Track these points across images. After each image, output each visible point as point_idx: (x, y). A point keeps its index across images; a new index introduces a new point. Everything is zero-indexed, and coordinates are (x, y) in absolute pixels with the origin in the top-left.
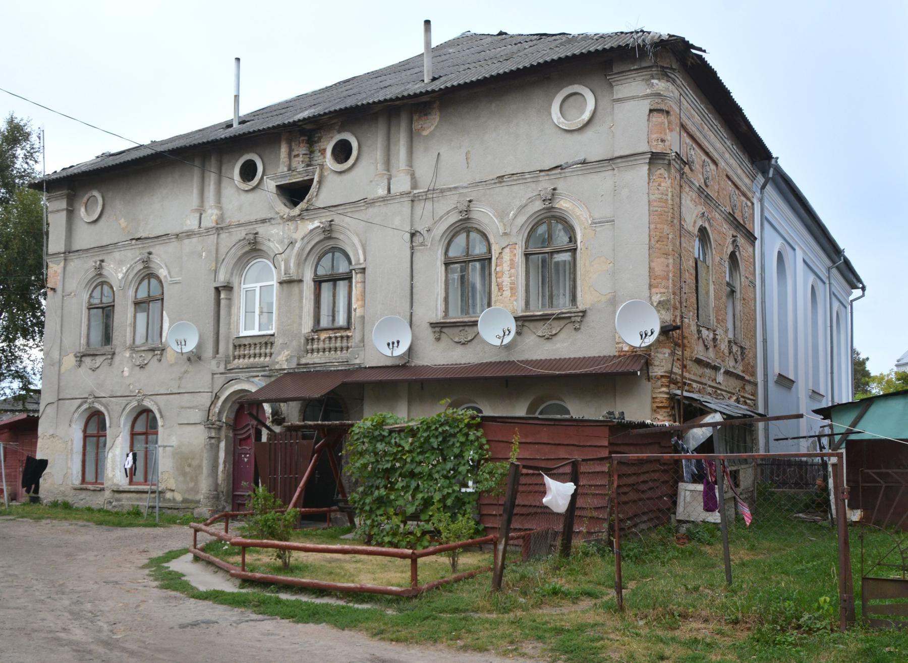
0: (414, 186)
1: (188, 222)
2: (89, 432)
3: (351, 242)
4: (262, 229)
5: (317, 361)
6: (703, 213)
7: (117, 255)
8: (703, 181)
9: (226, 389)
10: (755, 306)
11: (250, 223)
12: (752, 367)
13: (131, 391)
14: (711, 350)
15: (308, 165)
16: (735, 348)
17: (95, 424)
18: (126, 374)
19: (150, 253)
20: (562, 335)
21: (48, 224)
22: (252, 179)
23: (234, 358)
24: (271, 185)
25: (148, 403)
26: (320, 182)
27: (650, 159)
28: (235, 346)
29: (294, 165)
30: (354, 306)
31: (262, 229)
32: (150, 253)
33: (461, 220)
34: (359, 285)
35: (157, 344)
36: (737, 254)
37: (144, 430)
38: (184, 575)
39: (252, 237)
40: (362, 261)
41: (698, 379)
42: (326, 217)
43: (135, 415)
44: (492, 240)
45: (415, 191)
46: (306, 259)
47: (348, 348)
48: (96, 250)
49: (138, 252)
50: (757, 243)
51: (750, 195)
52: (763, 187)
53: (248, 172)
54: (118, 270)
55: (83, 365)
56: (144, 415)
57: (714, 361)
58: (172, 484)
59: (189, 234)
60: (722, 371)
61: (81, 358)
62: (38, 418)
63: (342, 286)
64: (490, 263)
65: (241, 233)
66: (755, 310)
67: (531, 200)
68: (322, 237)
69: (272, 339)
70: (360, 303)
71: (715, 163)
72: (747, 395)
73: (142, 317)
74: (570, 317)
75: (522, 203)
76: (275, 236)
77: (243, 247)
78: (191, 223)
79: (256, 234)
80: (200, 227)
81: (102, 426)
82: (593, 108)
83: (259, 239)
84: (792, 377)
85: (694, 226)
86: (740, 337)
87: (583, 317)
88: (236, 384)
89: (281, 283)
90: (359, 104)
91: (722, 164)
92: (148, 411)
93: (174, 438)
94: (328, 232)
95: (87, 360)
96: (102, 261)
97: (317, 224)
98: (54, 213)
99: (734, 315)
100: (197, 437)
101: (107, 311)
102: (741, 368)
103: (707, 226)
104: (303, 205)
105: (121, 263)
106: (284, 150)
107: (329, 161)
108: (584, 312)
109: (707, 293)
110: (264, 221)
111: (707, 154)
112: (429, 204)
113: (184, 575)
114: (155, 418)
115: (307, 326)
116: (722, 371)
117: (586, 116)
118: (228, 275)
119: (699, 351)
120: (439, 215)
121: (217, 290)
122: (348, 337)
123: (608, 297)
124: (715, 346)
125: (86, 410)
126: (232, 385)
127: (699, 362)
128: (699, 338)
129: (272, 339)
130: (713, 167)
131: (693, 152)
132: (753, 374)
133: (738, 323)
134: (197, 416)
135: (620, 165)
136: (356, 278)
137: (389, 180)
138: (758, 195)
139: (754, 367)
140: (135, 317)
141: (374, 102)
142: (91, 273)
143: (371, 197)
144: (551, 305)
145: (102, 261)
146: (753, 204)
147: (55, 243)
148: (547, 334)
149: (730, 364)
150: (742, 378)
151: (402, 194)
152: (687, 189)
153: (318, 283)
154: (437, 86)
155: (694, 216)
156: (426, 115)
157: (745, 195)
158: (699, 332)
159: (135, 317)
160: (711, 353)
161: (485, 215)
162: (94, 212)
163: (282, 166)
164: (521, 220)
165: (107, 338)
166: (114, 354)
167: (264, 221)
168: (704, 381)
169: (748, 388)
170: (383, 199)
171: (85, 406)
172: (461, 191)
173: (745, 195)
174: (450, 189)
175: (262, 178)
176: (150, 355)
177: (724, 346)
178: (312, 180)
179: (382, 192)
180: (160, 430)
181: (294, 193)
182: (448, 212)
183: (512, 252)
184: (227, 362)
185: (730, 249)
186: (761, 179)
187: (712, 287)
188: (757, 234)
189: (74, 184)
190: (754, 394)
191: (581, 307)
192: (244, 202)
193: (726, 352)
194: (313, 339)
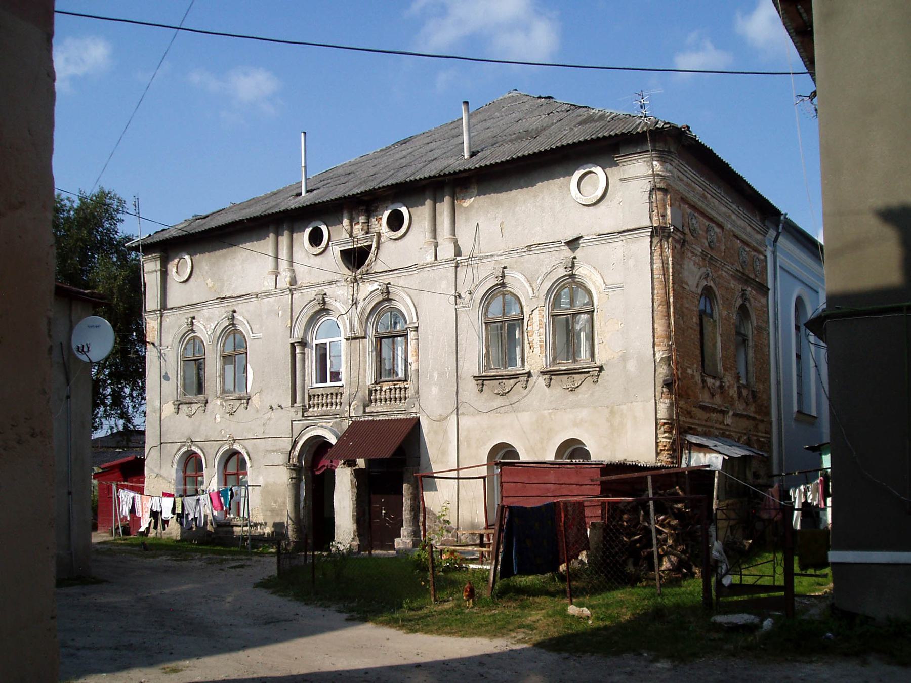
0: (458, 253)
1: (266, 283)
2: (188, 473)
3: (403, 303)
4: (328, 290)
5: (380, 409)
6: (708, 274)
7: (206, 312)
8: (707, 244)
9: (304, 434)
10: (769, 351)
11: (319, 285)
12: (766, 407)
13: (223, 436)
14: (717, 396)
15: (367, 233)
16: (745, 392)
17: (191, 464)
18: (218, 420)
19: (234, 311)
20: (583, 387)
21: (145, 284)
22: (320, 245)
23: (310, 407)
24: (336, 250)
25: (237, 447)
26: (378, 248)
27: (652, 232)
28: (310, 396)
29: (355, 232)
30: (410, 361)
31: (328, 290)
32: (234, 311)
33: (497, 285)
34: (414, 342)
35: (243, 394)
36: (748, 305)
37: (235, 471)
38: (347, 620)
39: (321, 297)
40: (415, 320)
41: (704, 423)
42: (385, 279)
43: (227, 457)
44: (524, 304)
45: (458, 258)
46: (368, 318)
47: (406, 398)
48: (187, 307)
49: (223, 310)
50: (771, 293)
51: (762, 249)
52: (776, 240)
53: (316, 238)
54: (207, 327)
55: (180, 411)
56: (235, 458)
57: (719, 406)
58: (260, 519)
59: (267, 294)
60: (731, 413)
61: (178, 406)
62: (144, 460)
63: (470, 268)
64: (523, 323)
65: (312, 293)
66: (769, 355)
67: (555, 268)
68: (381, 298)
69: (341, 390)
70: (414, 358)
71: (720, 226)
72: (760, 434)
73: (229, 369)
74: (588, 372)
75: (552, 264)
76: (339, 296)
77: (314, 306)
78: (269, 284)
79: (325, 294)
80: (436, 258)
81: (199, 467)
82: (605, 185)
83: (327, 300)
84: (814, 414)
85: (697, 287)
86: (752, 381)
87: (529, 377)
88: (312, 430)
89: (347, 339)
90: (408, 180)
91: (728, 226)
92: (237, 453)
93: (261, 478)
94: (387, 295)
95: (184, 407)
96: (193, 318)
97: (375, 286)
98: (150, 268)
99: (746, 363)
100: (282, 478)
101: (200, 364)
102: (752, 409)
103: (711, 284)
104: (364, 268)
105: (209, 319)
106: (346, 222)
107: (384, 228)
108: (601, 368)
109: (715, 345)
110: (330, 283)
111: (711, 219)
112: (470, 269)
113: (347, 620)
114: (244, 460)
115: (369, 377)
116: (731, 413)
117: (599, 193)
118: (302, 332)
119: (705, 398)
120: (482, 277)
121: (292, 344)
122: (406, 388)
123: (620, 354)
124: (722, 393)
125: (185, 453)
126: (308, 431)
127: (704, 408)
128: (703, 387)
129: (341, 390)
130: (718, 230)
131: (694, 221)
132: (768, 414)
133: (751, 369)
134: (281, 458)
135: (627, 237)
136: (411, 335)
137: (436, 246)
138: (770, 248)
139: (768, 407)
140: (224, 368)
141: (420, 179)
142: (184, 328)
143: (420, 263)
144: (575, 361)
145: (193, 318)
146: (766, 257)
147: (152, 301)
148: (570, 386)
149: (740, 407)
150: (754, 419)
151: (447, 261)
152: (690, 255)
153: (379, 339)
154: (476, 163)
155: (698, 277)
156: (466, 188)
157: (756, 250)
158: (704, 381)
159: (224, 368)
160: (718, 399)
161: (517, 283)
162: (184, 272)
163: (342, 234)
164: (547, 285)
165: (200, 389)
166: (207, 402)
167: (330, 283)
168: (708, 424)
169: (761, 427)
170: (431, 265)
171: (184, 449)
172: (497, 258)
173: (756, 250)
174: (487, 257)
175: (328, 244)
176: (238, 403)
177: (733, 392)
178: (371, 246)
179: (430, 258)
180: (249, 470)
181: (356, 258)
182: (486, 277)
183: (540, 313)
184: (304, 410)
185: (739, 302)
186: (772, 233)
187: (719, 339)
188: (770, 286)
189: (168, 247)
190: (769, 432)
191: (598, 363)
192: (314, 264)
193: (736, 396)
194: (376, 390)
